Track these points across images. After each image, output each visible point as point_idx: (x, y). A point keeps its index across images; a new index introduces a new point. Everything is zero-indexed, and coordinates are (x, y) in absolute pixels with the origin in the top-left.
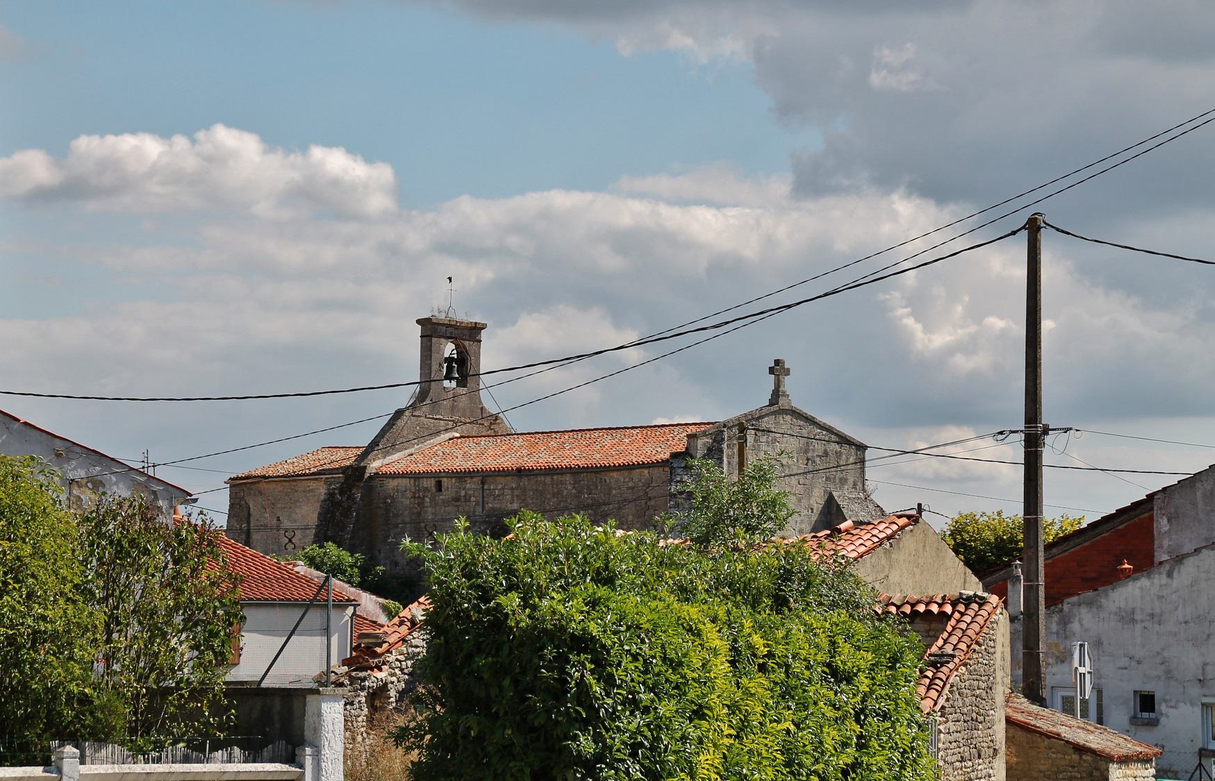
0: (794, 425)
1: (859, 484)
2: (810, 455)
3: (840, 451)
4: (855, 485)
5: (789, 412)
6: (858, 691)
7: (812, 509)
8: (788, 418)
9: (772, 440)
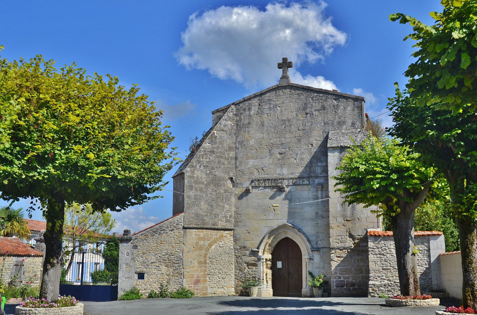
0: (293, 94)
1: (358, 123)
2: (308, 111)
3: (337, 105)
4: (353, 124)
5: (287, 87)
6: (45, 148)
7: (312, 145)
8: (287, 91)
9: (274, 106)
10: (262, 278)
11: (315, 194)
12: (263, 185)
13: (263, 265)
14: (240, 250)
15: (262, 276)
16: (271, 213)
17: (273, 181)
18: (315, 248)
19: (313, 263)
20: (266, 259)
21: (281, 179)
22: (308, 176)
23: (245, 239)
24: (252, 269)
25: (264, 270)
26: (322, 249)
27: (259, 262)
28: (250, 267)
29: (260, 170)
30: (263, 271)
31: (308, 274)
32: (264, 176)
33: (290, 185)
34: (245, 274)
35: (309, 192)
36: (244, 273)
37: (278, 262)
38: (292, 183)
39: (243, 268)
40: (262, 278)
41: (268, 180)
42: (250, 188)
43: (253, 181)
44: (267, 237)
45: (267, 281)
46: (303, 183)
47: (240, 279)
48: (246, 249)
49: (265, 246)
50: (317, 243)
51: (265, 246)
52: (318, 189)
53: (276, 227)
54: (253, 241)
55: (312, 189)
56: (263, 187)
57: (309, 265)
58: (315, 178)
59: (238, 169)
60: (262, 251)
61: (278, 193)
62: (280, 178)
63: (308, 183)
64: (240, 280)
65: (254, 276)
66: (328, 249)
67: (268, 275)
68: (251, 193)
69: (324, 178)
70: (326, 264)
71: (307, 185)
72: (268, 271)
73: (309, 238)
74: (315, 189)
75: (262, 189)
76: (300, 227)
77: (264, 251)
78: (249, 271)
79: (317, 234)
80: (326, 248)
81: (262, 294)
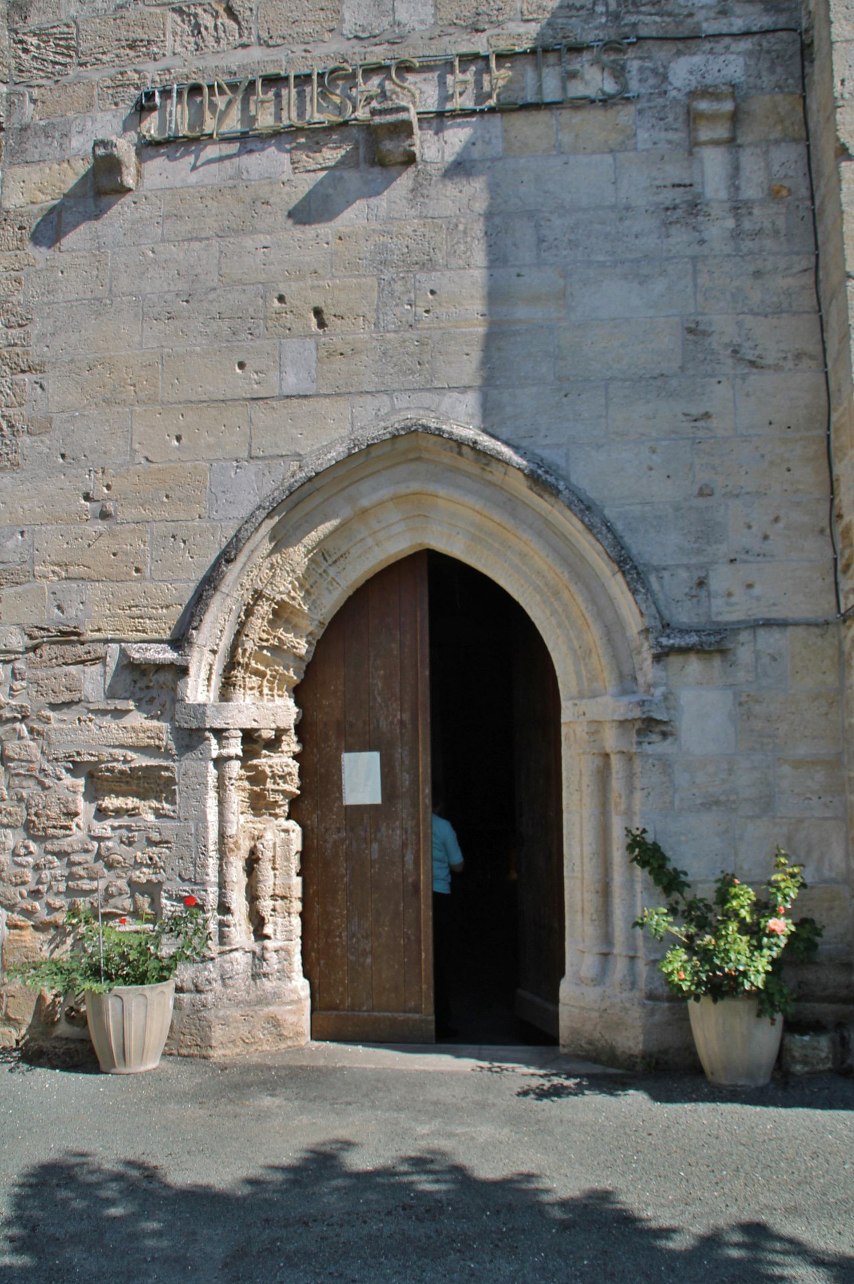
10: (212, 897)
11: (675, 172)
12: (233, 123)
13: (221, 787)
14: (31, 665)
15: (213, 876)
16: (292, 346)
17: (313, 90)
18: (684, 631)
19: (665, 765)
20: (249, 737)
21: (379, 69)
22: (612, 33)
23: (74, 570)
24: (125, 821)
25: (232, 830)
26: (744, 636)
27: (188, 762)
28: (111, 802)
29: (207, 20)
30: (222, 835)
31: (619, 855)
32: (235, 59)
33: (455, 114)
34: (71, 864)
35: (620, 156)
36: (60, 854)
37: (378, 801)
38: (481, 97)
39: (54, 811)
40: (212, 897)
41: (274, 81)
42: (125, 148)
43: (150, 96)
44: (261, 542)
45: (257, 922)
46: (564, 89)
47: (26, 904)
48: (80, 650)
49: (242, 625)
50: (701, 584)
51: (242, 625)
52: (704, 134)
53: (338, 452)
54: (136, 587)
55: (643, 135)
56: (227, 139)
57: (630, 776)
58: (671, 48)
59: (35, 21)
60: (218, 668)
61: (353, 178)
62: (372, 59)
63: (610, 87)
64: (28, 913)
65: (143, 875)
66: (800, 631)
67: (265, 869)
68: (128, 199)
69: (745, 45)
70: (786, 769)
71: (606, 101)
72: (269, 836)
73: (628, 540)
74: (671, 135)
75: (221, 159)
76: (545, 453)
77: (231, 665)
78: (100, 839)
79: (702, 502)
80: (783, 624)
81: (218, 1034)
